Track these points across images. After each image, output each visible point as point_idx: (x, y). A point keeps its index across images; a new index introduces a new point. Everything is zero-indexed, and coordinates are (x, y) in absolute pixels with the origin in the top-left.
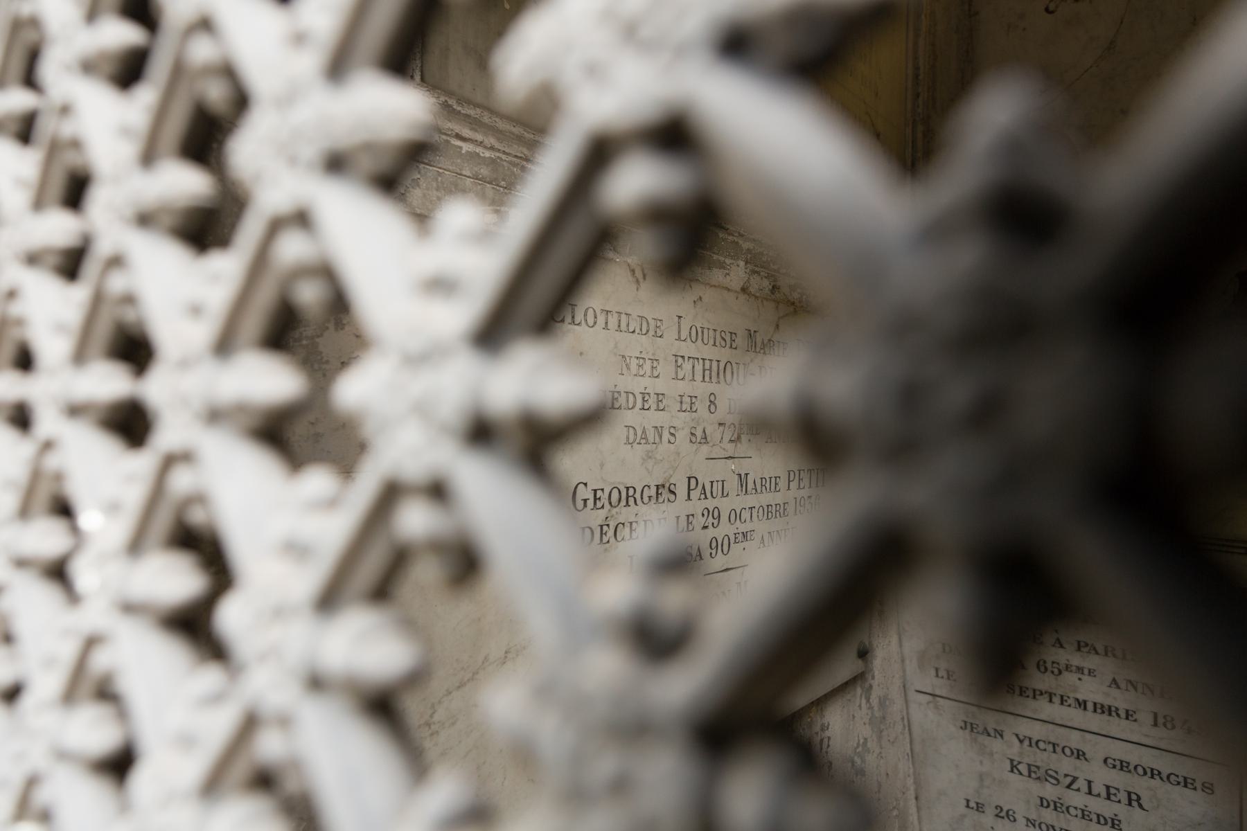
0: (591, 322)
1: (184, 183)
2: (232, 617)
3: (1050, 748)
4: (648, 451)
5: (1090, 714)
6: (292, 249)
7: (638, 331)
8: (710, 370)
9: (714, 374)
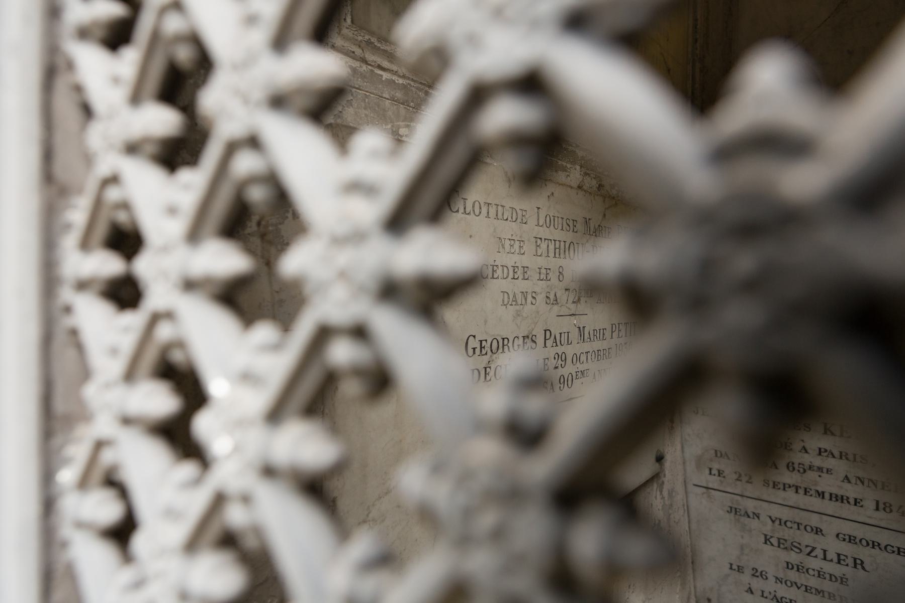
0: (477, 212)
1: (161, 120)
2: (204, 425)
3: (796, 526)
4: (517, 311)
5: (826, 501)
6: (246, 164)
7: (510, 219)
8: (559, 248)
9: (562, 251)
